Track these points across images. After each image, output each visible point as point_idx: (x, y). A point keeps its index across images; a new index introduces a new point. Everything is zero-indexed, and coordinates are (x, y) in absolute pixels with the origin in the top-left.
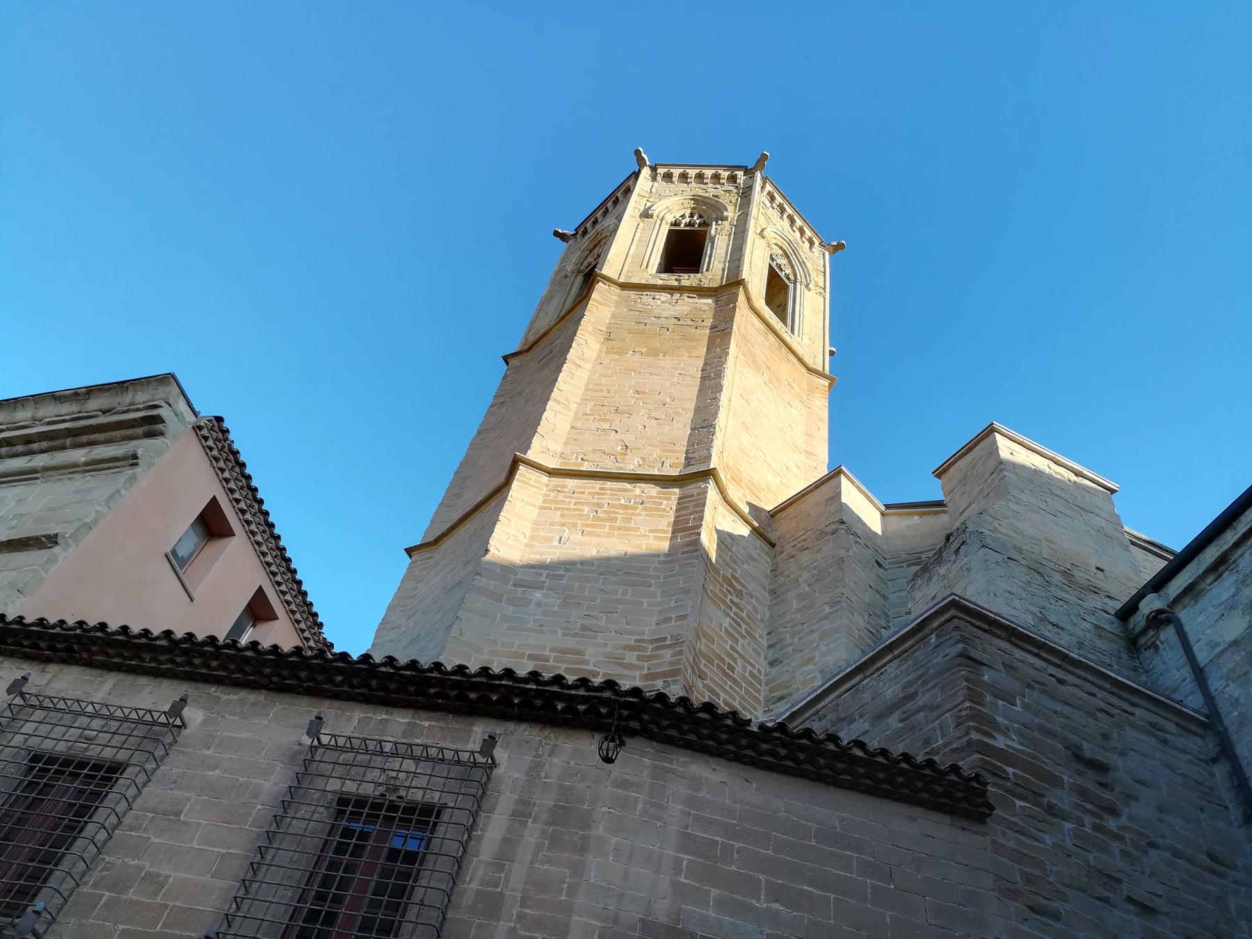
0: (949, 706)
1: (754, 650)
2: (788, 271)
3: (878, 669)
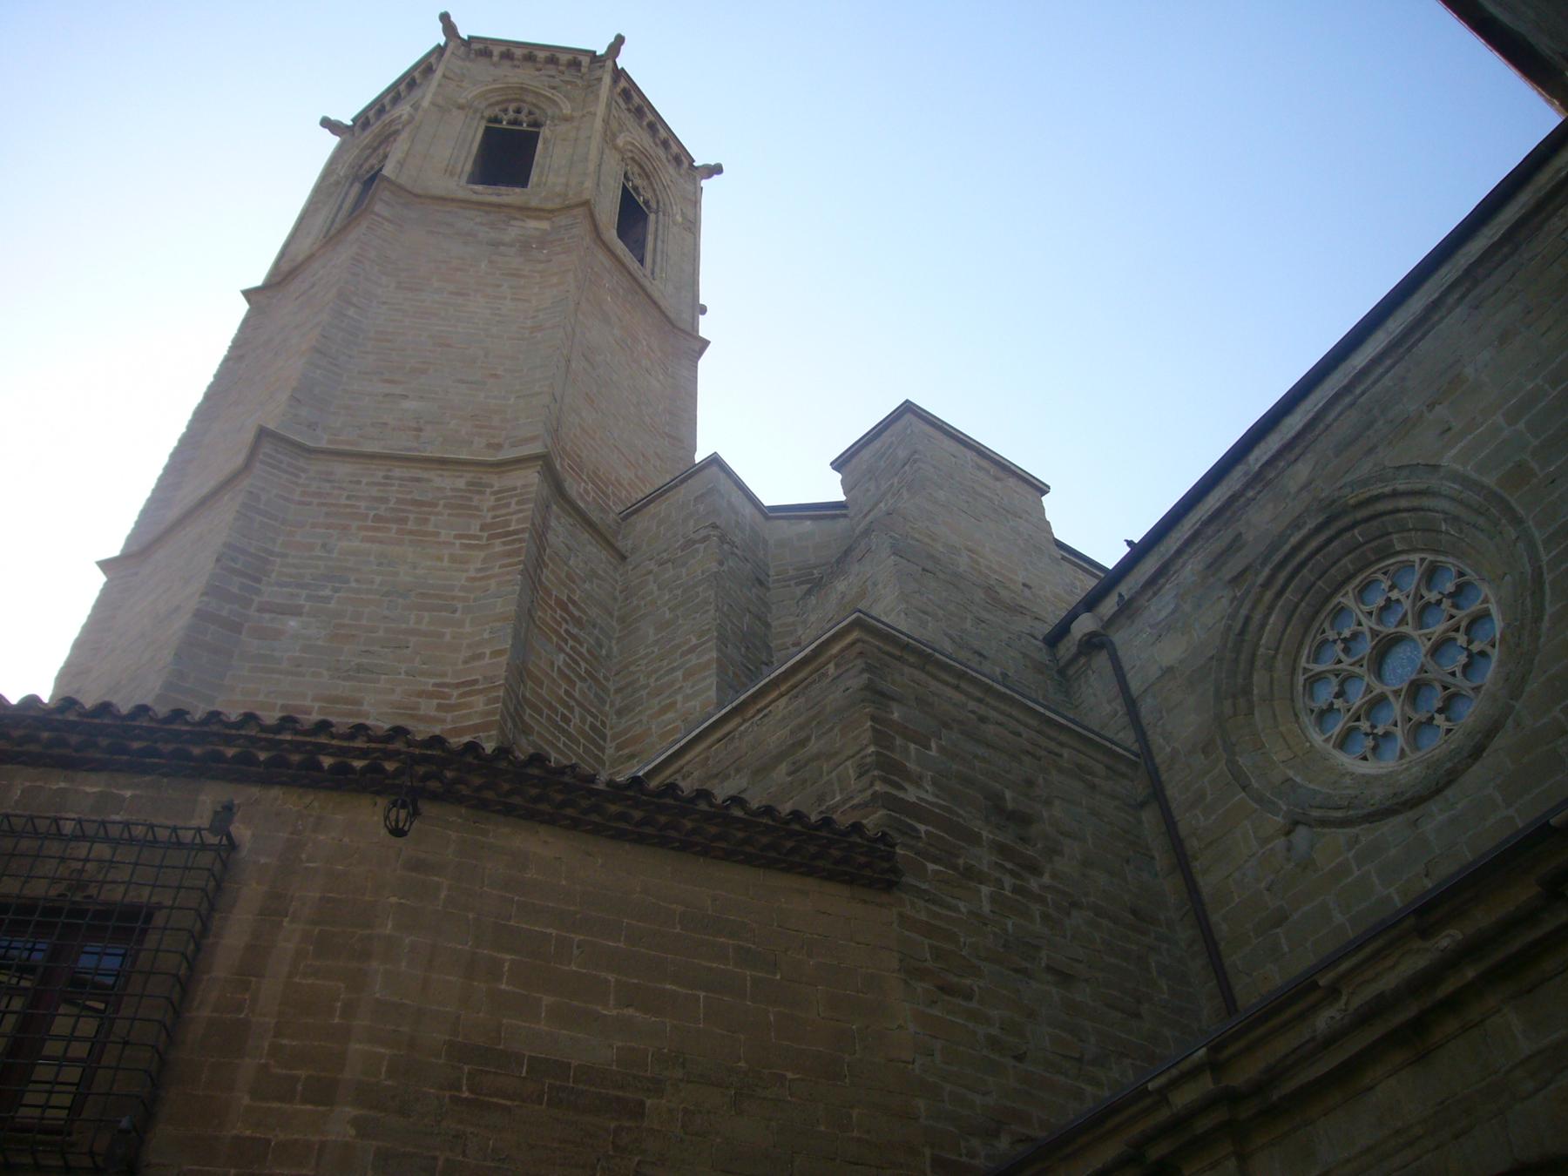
0: (851, 752)
1: (596, 695)
2: (649, 195)
3: (759, 711)
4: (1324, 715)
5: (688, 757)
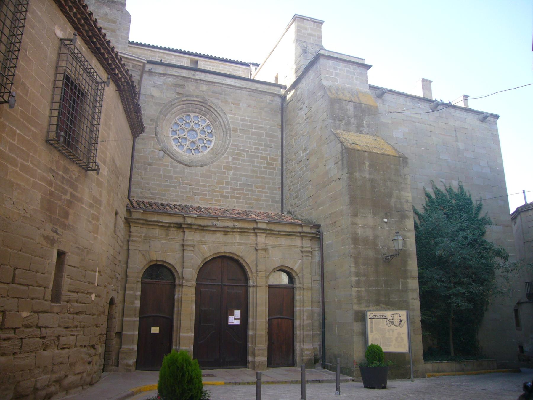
4: (174, 132)
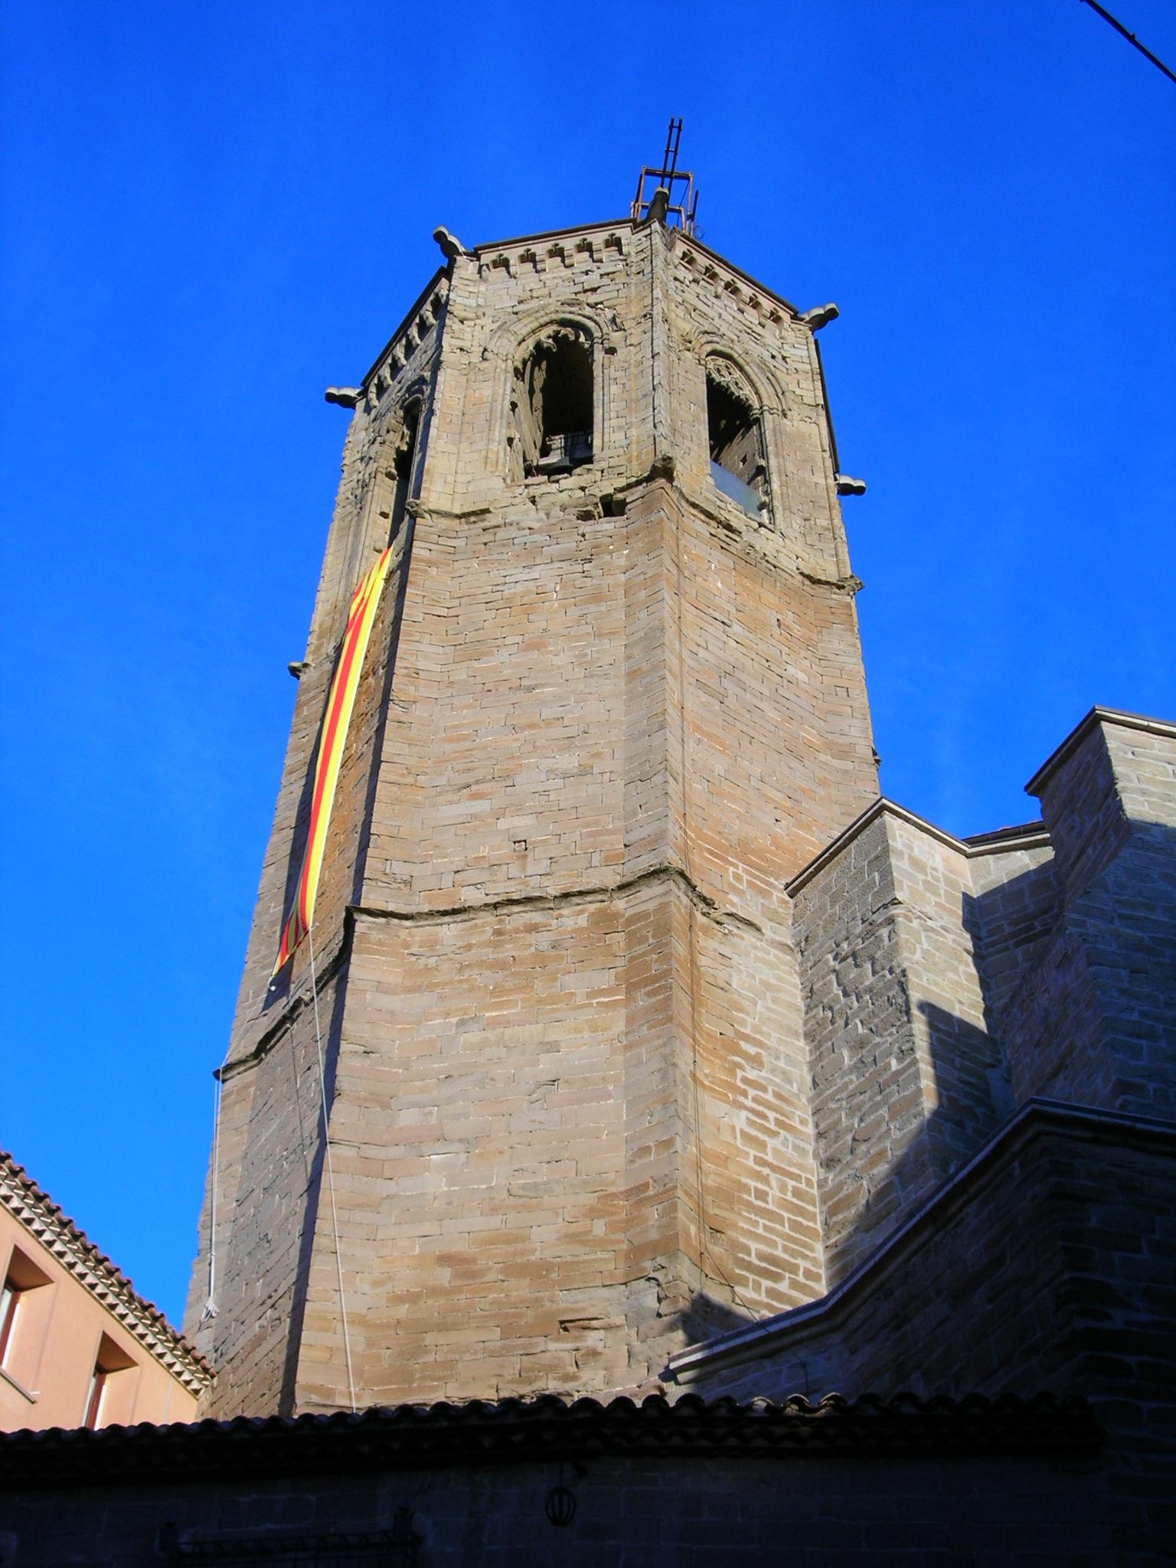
1: (796, 1147)
3: (951, 1218)
5: (885, 1274)
